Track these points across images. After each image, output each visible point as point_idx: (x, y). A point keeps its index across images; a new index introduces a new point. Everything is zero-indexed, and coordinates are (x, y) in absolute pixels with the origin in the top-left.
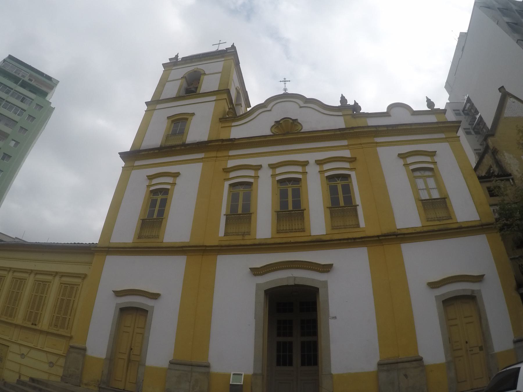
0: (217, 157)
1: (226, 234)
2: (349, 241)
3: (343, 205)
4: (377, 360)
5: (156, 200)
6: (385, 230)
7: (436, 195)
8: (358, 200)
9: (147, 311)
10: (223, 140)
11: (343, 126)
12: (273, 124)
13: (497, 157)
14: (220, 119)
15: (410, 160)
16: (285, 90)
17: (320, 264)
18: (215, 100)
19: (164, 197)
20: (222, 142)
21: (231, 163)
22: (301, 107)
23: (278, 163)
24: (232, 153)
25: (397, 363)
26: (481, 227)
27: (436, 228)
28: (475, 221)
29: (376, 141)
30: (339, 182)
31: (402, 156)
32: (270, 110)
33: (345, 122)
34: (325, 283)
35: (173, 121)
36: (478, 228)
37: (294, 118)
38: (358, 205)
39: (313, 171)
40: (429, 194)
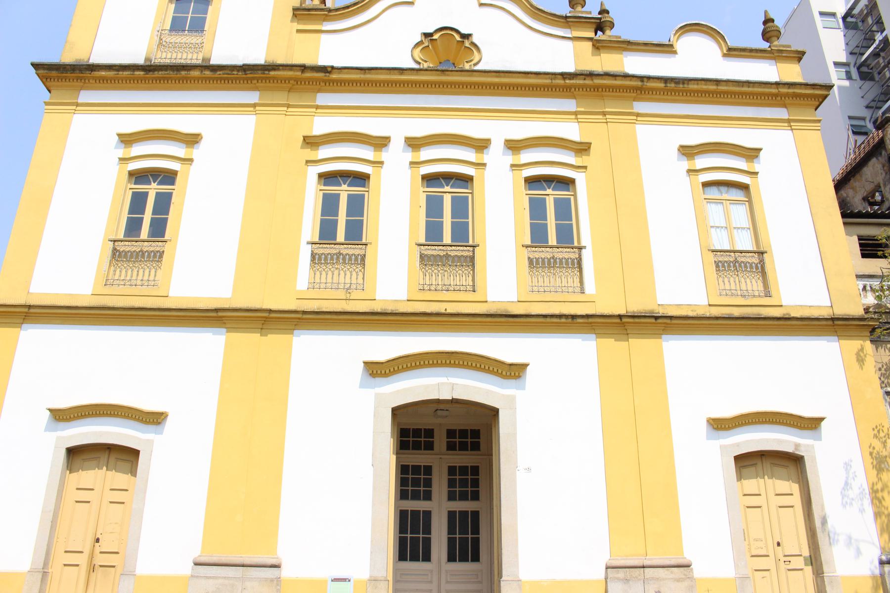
0: (288, 106)
1: (312, 286)
2: (563, 320)
3: (555, 243)
4: (605, 558)
5: (145, 195)
6: (636, 306)
7: (745, 242)
8: (586, 234)
9: (135, 453)
10: (304, 68)
11: (570, 67)
12: (418, 39)
14: (295, 9)
15: (701, 162)
17: (503, 363)
19: (165, 188)
20: (303, 72)
21: (322, 125)
23: (728, 81)
24: (323, 99)
25: (643, 567)
26: (830, 323)
27: (736, 312)
28: (819, 307)
29: (635, 111)
30: (549, 191)
31: (688, 152)
33: (577, 56)
34: (512, 399)
36: (824, 323)
37: (464, 31)
38: (585, 247)
39: (497, 159)
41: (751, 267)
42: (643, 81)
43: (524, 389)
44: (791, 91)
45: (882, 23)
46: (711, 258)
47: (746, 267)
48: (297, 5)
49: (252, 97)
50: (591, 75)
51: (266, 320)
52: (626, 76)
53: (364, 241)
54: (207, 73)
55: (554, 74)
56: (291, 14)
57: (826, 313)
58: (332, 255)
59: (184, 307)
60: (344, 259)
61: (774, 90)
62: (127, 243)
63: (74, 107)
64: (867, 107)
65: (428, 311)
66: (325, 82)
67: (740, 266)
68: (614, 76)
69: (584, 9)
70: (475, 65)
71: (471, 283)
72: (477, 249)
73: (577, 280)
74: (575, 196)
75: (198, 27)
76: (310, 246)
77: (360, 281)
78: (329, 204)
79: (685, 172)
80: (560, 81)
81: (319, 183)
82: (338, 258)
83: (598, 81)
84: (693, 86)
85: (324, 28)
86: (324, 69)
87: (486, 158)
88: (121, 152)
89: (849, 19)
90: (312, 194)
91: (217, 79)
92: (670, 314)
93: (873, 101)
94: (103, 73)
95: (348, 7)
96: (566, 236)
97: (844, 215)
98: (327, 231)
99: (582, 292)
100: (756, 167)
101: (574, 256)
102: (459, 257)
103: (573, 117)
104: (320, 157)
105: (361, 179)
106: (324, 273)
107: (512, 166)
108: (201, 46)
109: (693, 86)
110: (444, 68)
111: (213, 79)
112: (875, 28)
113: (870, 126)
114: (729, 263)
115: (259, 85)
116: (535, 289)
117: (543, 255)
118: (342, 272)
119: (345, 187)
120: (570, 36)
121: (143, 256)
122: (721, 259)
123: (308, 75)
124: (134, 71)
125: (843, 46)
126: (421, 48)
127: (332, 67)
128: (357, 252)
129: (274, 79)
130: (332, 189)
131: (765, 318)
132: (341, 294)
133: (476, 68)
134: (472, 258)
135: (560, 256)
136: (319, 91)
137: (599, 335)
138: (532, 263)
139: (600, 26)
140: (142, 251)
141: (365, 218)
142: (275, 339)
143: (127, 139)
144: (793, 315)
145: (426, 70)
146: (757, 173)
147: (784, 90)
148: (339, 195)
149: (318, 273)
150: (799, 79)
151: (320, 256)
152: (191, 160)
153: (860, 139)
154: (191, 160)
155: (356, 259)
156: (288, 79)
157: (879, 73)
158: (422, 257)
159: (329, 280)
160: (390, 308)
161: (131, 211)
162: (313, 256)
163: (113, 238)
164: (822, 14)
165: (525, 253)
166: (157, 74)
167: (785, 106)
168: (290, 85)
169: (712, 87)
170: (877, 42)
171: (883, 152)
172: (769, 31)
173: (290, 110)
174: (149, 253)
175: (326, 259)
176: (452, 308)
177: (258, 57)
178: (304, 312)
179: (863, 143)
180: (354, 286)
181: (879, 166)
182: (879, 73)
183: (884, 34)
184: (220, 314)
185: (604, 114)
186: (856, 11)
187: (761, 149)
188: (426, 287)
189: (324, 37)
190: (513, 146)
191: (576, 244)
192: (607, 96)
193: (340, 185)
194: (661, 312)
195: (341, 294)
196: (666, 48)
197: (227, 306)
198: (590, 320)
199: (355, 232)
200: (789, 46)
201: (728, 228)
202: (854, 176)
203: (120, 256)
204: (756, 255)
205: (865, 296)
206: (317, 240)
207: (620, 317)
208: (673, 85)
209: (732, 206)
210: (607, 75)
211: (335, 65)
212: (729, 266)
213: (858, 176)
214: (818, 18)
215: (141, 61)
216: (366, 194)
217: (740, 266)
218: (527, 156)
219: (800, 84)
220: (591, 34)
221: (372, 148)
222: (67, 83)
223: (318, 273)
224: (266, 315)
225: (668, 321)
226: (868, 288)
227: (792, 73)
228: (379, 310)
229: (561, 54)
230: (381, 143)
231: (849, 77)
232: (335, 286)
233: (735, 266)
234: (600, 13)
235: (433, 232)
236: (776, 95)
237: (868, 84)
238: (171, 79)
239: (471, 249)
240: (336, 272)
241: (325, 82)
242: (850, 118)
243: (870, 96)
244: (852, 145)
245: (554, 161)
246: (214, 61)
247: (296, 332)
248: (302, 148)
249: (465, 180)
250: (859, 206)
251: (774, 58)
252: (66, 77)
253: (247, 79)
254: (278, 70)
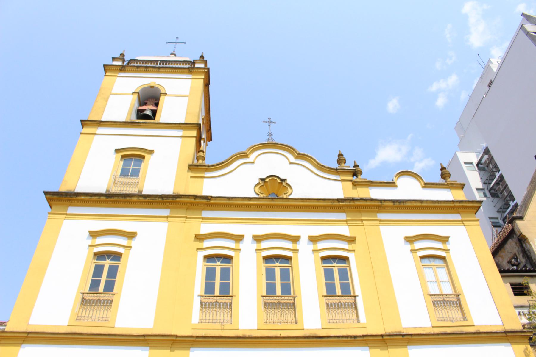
0: (186, 218)
2: (349, 339)
5: (102, 267)
6: (390, 329)
7: (447, 289)
8: (357, 288)
10: (195, 197)
12: (257, 181)
13: (524, 245)
14: (190, 165)
16: (270, 134)
18: (181, 137)
19: (114, 263)
20: (195, 199)
21: (206, 228)
22: (291, 163)
23: (427, 201)
24: (206, 214)
26: (504, 335)
27: (449, 330)
28: (496, 325)
30: (335, 264)
31: (410, 240)
33: (344, 190)
35: (123, 157)
37: (282, 177)
38: (358, 296)
39: (305, 248)
40: (440, 288)
41: (453, 303)
42: (381, 202)
44: (461, 205)
45: (498, 167)
46: (430, 299)
47: (450, 303)
48: (191, 163)
49: (166, 212)
50: (353, 200)
51: (174, 342)
52: (372, 200)
53: (231, 295)
54: (141, 199)
55: (333, 200)
56: (187, 168)
57: (500, 329)
58: (213, 303)
59: (124, 333)
60: (220, 305)
61: (452, 205)
62: (91, 295)
63: (65, 216)
64: (498, 212)
65: (270, 335)
66: (207, 205)
67: (447, 303)
68: (366, 200)
69: (346, 165)
70: (289, 195)
71: (294, 319)
72: (296, 299)
73: (355, 315)
74: (350, 266)
75: (136, 173)
76: (200, 297)
77: (229, 318)
78: (210, 274)
80: (336, 204)
81: (204, 261)
82: (216, 305)
83: (357, 203)
84: (408, 204)
85: (205, 176)
86: (206, 198)
87: (298, 246)
88: (90, 242)
89: (480, 166)
90: (200, 267)
91: (146, 202)
92: (410, 333)
93: (501, 208)
94: (83, 198)
95: (219, 165)
96: (346, 289)
97: (501, 271)
98: (209, 289)
99: (358, 321)
100: (448, 247)
101: (351, 300)
102: (286, 303)
103: (345, 223)
104: (204, 247)
105: (228, 259)
106: (208, 314)
107: (313, 250)
108: (137, 184)
109: (408, 204)
110: (273, 197)
111: (144, 202)
112: (494, 170)
113: (501, 222)
114: (440, 301)
115: (170, 206)
116: (331, 321)
117: (334, 301)
118: (218, 313)
119: (219, 263)
120: (339, 179)
121: (100, 303)
122: (435, 300)
123: (198, 201)
124: (100, 196)
125: (480, 180)
126: (259, 186)
127: (211, 197)
128: (227, 301)
129: (179, 203)
130: (211, 265)
131: (466, 333)
132: (218, 326)
133: (290, 197)
134: (294, 304)
135: (344, 301)
136: (204, 209)
137: (370, 347)
138: (329, 306)
139: (355, 174)
140: (99, 299)
141: (231, 281)
143: (94, 235)
144: (481, 331)
145: (263, 198)
146: (449, 250)
147: (457, 204)
148: (215, 268)
149: (204, 314)
150: (464, 198)
151: (205, 303)
152: (130, 247)
153: (499, 229)
154: (130, 247)
155: (227, 305)
156: (187, 203)
157: (501, 193)
158: (265, 304)
159: (211, 318)
160: (247, 334)
161: (94, 276)
162: (201, 303)
163: (82, 291)
164: (465, 163)
165: (324, 300)
166: (113, 199)
167: (459, 213)
168: (187, 206)
169: (419, 204)
170: (497, 177)
171: (515, 236)
172: (445, 174)
173: (187, 220)
174: (104, 300)
175: (209, 305)
176: (284, 334)
177: (169, 190)
178: (197, 337)
179: (501, 231)
180: (225, 321)
181: (514, 244)
182: (501, 193)
183: (500, 173)
184: (146, 338)
185: (362, 220)
186: (483, 161)
187: (449, 237)
188: (268, 321)
189: (205, 180)
190: (313, 239)
191: (352, 294)
193: (216, 262)
194: (405, 332)
195: (218, 326)
196: (392, 184)
197: (150, 333)
198: (365, 338)
199: (225, 289)
200: (456, 181)
201: (437, 281)
202: (500, 250)
203: (86, 302)
204: (455, 297)
205: (521, 319)
206: (203, 294)
207: (382, 336)
208: (398, 204)
209: (438, 269)
210: (362, 199)
211: (213, 196)
212: (441, 303)
213: (502, 249)
214: (464, 166)
215: (104, 191)
216: (231, 267)
217: (447, 303)
218: (321, 245)
219: (465, 201)
220: (350, 178)
221: (234, 241)
222: (62, 203)
223: (204, 314)
224: (174, 338)
225: (410, 337)
226: (522, 313)
227: (460, 195)
228: (241, 335)
229: (336, 189)
230: (239, 238)
231: (485, 196)
232: (214, 321)
233: (444, 303)
234: (354, 167)
235: (271, 289)
236: (453, 207)
237: (496, 200)
238: (121, 201)
239: (293, 298)
240: (215, 313)
241: (207, 205)
242: (490, 218)
243: (499, 206)
244: (495, 233)
245: (337, 248)
246: (144, 192)
247: (191, 349)
248: (194, 241)
249: (287, 259)
250: (507, 267)
251: (449, 188)
252: (62, 199)
253: (164, 203)
254: (181, 198)
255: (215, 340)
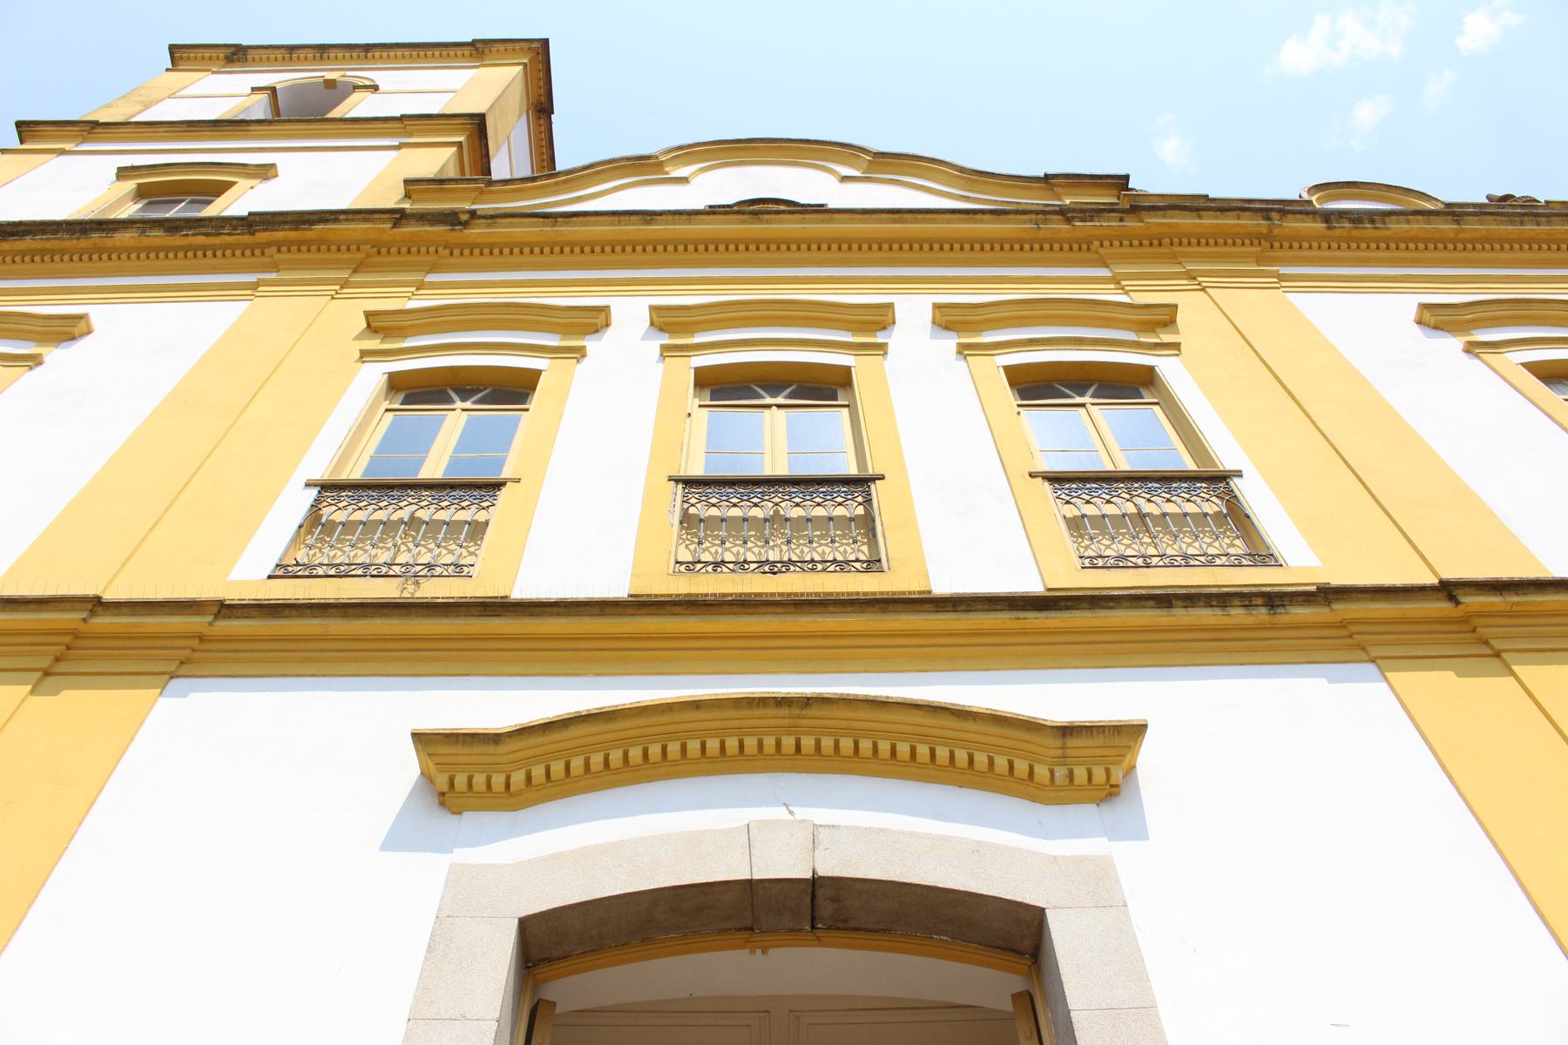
1: (283, 572)
2: (1237, 614)
32: (684, 180)
34: (1101, 889)
38: (1239, 474)
43: (1139, 832)
79: (1464, 355)
142: (81, 706)
166: (28, 243)
168: (359, 256)
192: (1185, 255)
224: (71, 618)
238: (62, 252)
241: (450, 248)
254: (336, 221)
255: (337, 626)
